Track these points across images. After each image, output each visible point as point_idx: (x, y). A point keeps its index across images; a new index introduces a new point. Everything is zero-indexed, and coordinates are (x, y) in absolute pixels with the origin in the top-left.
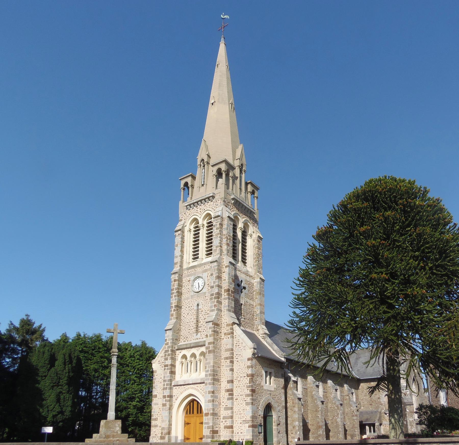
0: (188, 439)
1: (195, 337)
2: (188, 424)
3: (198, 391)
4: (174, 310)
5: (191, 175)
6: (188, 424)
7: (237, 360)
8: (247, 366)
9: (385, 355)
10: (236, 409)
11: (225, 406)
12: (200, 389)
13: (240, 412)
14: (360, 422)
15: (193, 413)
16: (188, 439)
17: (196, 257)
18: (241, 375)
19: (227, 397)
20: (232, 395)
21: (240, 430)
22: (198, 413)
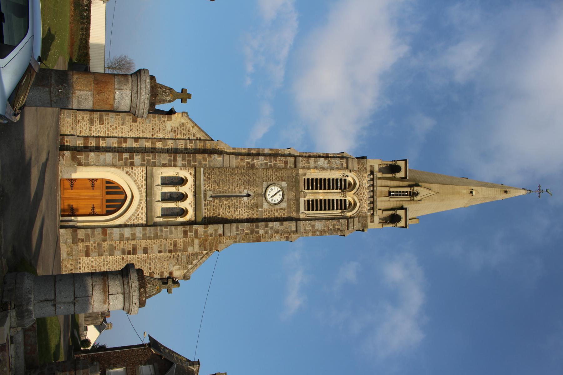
0: (72, 186)
1: (209, 193)
2: (93, 186)
3: (137, 210)
4: (248, 163)
5: (406, 178)
6: (93, 186)
7: (172, 257)
8: (162, 272)
9: (391, 212)
10: (111, 259)
11: (114, 245)
12: (139, 212)
13: (107, 265)
14: (65, 316)
15: (108, 193)
16: (72, 186)
17: (312, 184)
18: (152, 264)
19: (126, 248)
20: (129, 253)
21: (84, 265)
22: (108, 201)
